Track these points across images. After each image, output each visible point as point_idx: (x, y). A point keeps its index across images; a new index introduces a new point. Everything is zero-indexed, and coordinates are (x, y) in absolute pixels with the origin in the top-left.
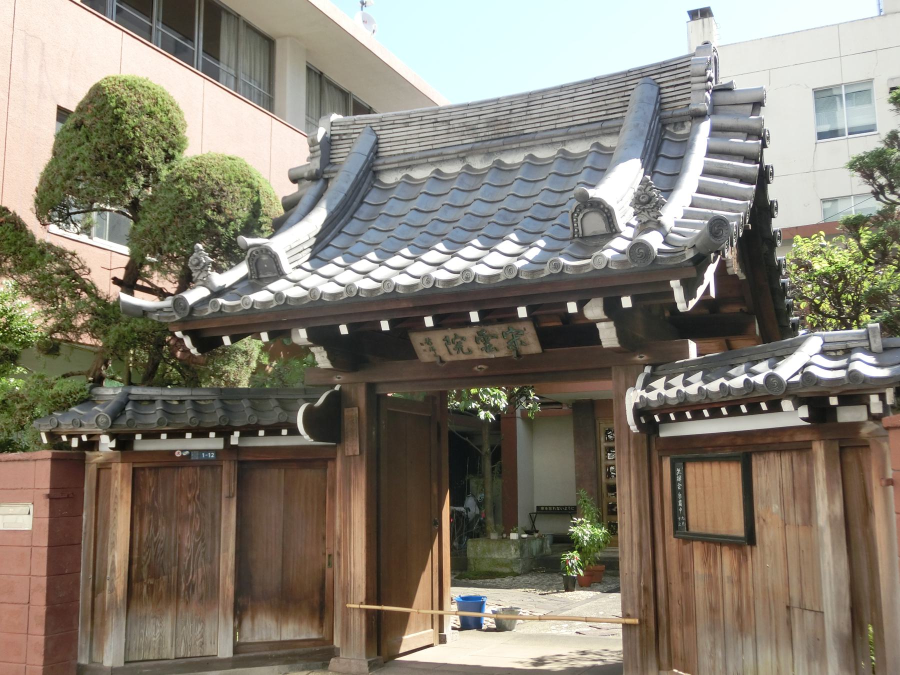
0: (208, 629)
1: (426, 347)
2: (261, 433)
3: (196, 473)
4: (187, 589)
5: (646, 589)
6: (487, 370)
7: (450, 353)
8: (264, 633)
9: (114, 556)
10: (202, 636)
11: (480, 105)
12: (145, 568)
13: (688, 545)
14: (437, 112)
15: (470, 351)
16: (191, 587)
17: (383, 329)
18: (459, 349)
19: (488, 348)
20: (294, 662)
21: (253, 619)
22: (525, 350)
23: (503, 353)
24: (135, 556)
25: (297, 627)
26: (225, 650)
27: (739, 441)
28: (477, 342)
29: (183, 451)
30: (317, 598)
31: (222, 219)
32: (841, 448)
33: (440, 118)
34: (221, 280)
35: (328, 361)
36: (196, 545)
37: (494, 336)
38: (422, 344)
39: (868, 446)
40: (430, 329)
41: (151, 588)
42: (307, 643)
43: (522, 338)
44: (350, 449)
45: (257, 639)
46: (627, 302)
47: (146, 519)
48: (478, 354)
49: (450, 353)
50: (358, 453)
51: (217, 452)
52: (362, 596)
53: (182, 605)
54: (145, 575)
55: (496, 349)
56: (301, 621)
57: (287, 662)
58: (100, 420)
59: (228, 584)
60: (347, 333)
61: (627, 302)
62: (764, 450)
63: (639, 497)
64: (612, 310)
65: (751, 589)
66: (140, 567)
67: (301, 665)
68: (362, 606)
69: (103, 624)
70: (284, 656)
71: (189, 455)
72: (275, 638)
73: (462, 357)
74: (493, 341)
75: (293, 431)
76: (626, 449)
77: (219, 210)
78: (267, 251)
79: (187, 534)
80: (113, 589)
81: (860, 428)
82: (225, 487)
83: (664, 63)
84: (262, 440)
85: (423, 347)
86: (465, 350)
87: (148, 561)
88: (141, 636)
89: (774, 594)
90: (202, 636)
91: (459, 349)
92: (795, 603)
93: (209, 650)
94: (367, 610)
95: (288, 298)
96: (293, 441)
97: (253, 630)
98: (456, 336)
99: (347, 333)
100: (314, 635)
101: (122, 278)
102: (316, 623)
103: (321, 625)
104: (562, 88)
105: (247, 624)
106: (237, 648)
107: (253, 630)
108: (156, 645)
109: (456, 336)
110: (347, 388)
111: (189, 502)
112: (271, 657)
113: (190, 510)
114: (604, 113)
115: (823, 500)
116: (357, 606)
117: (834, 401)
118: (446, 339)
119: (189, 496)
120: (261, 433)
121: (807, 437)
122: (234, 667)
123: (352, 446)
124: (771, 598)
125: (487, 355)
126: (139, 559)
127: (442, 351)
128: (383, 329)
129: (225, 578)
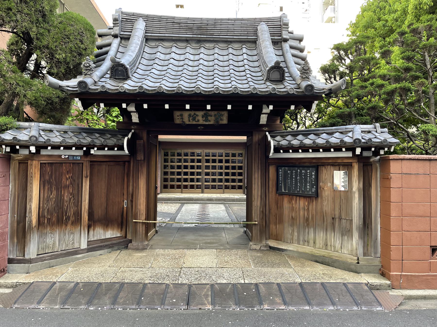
0: (76, 236)
1: (179, 117)
2: (49, 148)
3: (71, 166)
4: (66, 219)
6: (203, 129)
7: (189, 121)
8: (98, 236)
9: (31, 206)
10: (73, 240)
11: (194, 19)
12: (46, 210)
13: (281, 197)
15: (198, 121)
16: (68, 218)
17: (166, 108)
18: (194, 119)
20: (112, 247)
21: (94, 230)
23: (212, 123)
25: (112, 232)
26: (84, 246)
27: (314, 161)
28: (203, 118)
29: (65, 155)
32: (363, 165)
35: (138, 119)
36: (70, 199)
37: (211, 116)
38: (178, 116)
39: (372, 165)
40: (209, 110)
41: (49, 220)
42: (116, 238)
43: (222, 117)
44: (139, 157)
45: (95, 239)
46: (145, 106)
47: (46, 187)
48: (201, 122)
49: (189, 121)
50: (143, 159)
51: (81, 156)
52: (144, 217)
53: (64, 226)
54: (46, 214)
55: (210, 121)
56: (113, 230)
57: (110, 248)
58: (32, 138)
60: (168, 108)
61: (145, 106)
62: (324, 165)
63: (261, 179)
64: (139, 109)
65: (314, 212)
66: (44, 210)
68: (144, 221)
70: (109, 245)
71: (68, 158)
72: (103, 237)
73: (194, 123)
74: (209, 118)
75: (121, 148)
76: (257, 162)
77: (81, 41)
80: (31, 221)
81: (370, 159)
82: (84, 173)
83: (269, 18)
85: (178, 117)
86: (196, 120)
87: (48, 208)
88: (44, 242)
89: (326, 213)
90: (73, 240)
91: (194, 119)
92: (337, 216)
93: (76, 245)
94: (145, 223)
96: (120, 153)
97: (94, 235)
98: (195, 114)
99: (168, 108)
102: (120, 230)
103: (121, 230)
104: (229, 19)
105: (91, 232)
107: (94, 235)
108: (51, 246)
109: (195, 114)
110: (137, 131)
111: (67, 179)
112: (103, 246)
113: (68, 183)
114: (246, 33)
115: (356, 182)
116: (142, 221)
117: (18, 147)
119: (67, 176)
120: (106, 149)
121: (350, 161)
122: (87, 252)
124: (325, 215)
125: (205, 123)
126: (43, 206)
128: (166, 108)
129: (84, 213)
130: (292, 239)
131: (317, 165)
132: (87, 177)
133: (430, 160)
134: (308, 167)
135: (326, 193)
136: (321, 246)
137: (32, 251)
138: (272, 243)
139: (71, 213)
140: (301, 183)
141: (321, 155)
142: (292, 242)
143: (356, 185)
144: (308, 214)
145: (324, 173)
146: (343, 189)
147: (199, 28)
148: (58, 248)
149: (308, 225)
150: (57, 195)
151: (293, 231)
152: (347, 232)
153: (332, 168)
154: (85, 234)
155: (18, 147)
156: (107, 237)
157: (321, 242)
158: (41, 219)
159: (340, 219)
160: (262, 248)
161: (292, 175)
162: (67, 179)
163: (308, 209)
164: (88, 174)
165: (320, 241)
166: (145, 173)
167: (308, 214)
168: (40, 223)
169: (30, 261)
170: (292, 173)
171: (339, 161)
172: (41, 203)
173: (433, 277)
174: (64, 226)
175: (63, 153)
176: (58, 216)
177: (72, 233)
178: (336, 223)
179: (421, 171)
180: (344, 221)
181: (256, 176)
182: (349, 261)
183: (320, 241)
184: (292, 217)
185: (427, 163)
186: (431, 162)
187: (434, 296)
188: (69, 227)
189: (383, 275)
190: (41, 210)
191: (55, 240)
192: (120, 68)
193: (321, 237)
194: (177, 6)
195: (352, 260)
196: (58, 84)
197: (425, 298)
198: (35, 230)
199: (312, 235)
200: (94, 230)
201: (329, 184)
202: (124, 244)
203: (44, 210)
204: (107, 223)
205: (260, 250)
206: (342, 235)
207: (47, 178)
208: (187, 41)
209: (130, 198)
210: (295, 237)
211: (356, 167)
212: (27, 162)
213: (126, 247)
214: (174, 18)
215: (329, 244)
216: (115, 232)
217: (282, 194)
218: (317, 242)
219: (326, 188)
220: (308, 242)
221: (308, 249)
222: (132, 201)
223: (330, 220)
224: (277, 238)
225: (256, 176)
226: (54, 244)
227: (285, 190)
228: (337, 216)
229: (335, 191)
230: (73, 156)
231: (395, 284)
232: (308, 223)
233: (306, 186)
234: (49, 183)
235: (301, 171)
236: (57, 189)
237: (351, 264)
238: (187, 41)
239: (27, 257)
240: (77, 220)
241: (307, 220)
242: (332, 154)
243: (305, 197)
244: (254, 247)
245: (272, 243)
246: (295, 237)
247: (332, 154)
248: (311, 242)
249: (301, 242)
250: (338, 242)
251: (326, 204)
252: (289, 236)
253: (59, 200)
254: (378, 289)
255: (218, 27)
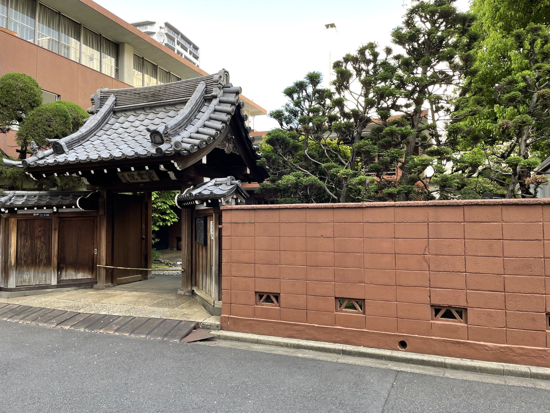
4: (39, 261)
5: (189, 260)
14: (136, 90)
15: (137, 179)
16: (41, 261)
19: (142, 178)
20: (80, 286)
21: (66, 271)
22: (154, 179)
23: (148, 180)
24: (19, 250)
26: (54, 282)
30: (91, 264)
31: (51, 129)
33: (137, 92)
34: (40, 154)
36: (42, 246)
41: (25, 261)
45: (67, 278)
47: (23, 238)
51: (50, 214)
52: (104, 263)
53: (37, 267)
56: (84, 273)
59: (55, 260)
67: (83, 287)
69: (8, 273)
72: (74, 278)
73: (135, 181)
75: (76, 207)
78: (58, 143)
79: (39, 243)
80: (11, 262)
82: (53, 226)
84: (64, 209)
91: (134, 178)
93: (48, 282)
95: (59, 162)
96: (76, 210)
97: (66, 275)
100: (90, 277)
101: (396, 104)
102: (91, 273)
103: (92, 273)
105: (64, 273)
106: (58, 282)
107: (66, 275)
111: (39, 231)
117: (16, 209)
118: (128, 175)
123: (101, 212)
126: (20, 251)
127: (128, 179)
132: (55, 230)
137: (12, 283)
139: (43, 256)
147: (153, 95)
148: (33, 283)
150: (32, 244)
154: (54, 274)
155: (16, 209)
156: (78, 278)
158: (19, 261)
160: (186, 294)
162: (39, 231)
164: (57, 227)
166: (105, 225)
169: (11, 290)
172: (19, 249)
173: (257, 323)
174: (37, 267)
175: (36, 212)
176: (32, 259)
177: (44, 272)
179: (247, 220)
181: (184, 227)
185: (252, 213)
186: (256, 211)
187: (246, 339)
188: (41, 268)
190: (19, 254)
191: (31, 277)
192: (58, 145)
194: (327, 26)
196: (11, 164)
197: (238, 340)
198: (14, 268)
200: (66, 271)
202: (89, 285)
203: (21, 254)
204: (77, 266)
207: (23, 230)
213: (92, 287)
216: (86, 274)
226: (30, 279)
230: (43, 214)
231: (224, 325)
234: (25, 234)
236: (32, 239)
239: (9, 287)
240: (48, 263)
253: (33, 247)
254: (208, 329)
255: (168, 91)
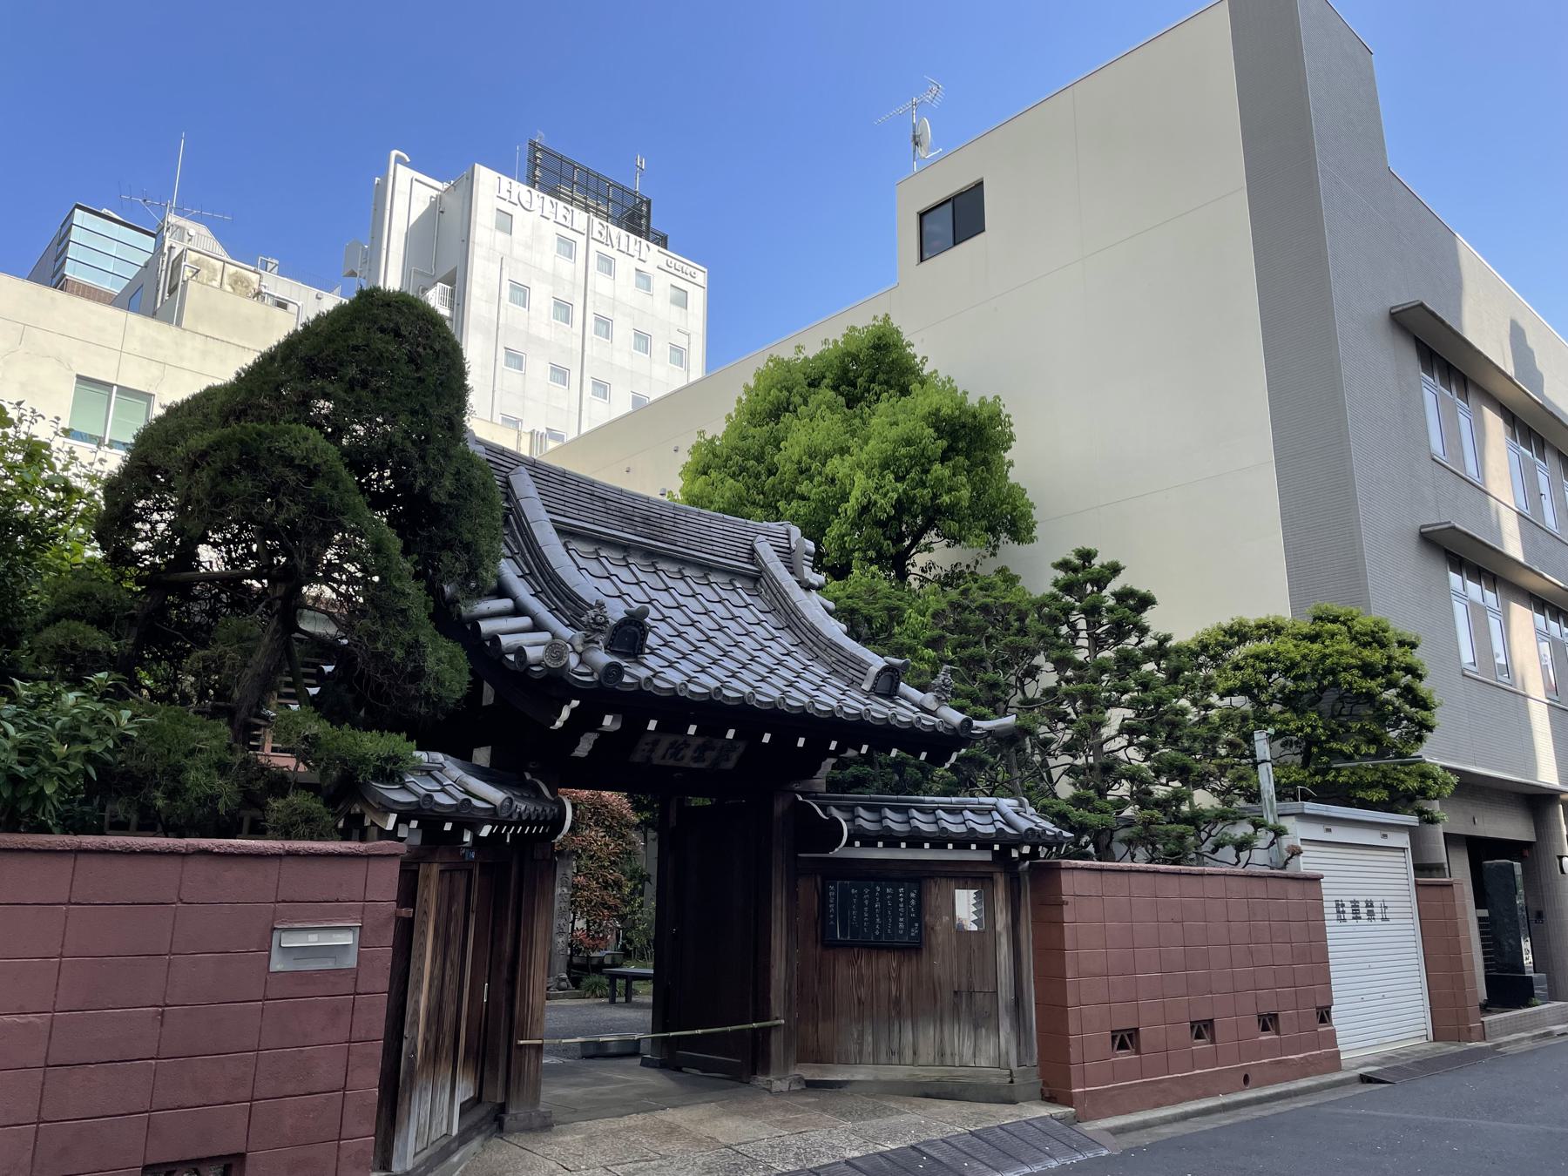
92: (964, 988)
130: (861, 1052)
131: (921, 875)
133: (1179, 874)
134: (900, 881)
135: (940, 937)
136: (931, 1059)
138: (811, 1073)
140: (883, 915)
141: (927, 854)
142: (860, 1062)
143: (1002, 920)
144: (899, 989)
145: (935, 893)
146: (974, 928)
149: (899, 1013)
151: (861, 1035)
152: (982, 1021)
153: (953, 884)
157: (931, 1050)
159: (971, 993)
161: (861, 899)
163: (899, 976)
165: (927, 1051)
167: (899, 989)
168: (433, 1055)
170: (861, 894)
171: (968, 869)
178: (967, 1004)
180: (979, 997)
181: (779, 901)
182: (994, 1080)
183: (927, 1051)
184: (859, 999)
189: (1050, 1098)
193: (928, 1039)
195: (998, 1078)
199: (908, 1036)
201: (946, 919)
205: (790, 1092)
206: (976, 1027)
208: (625, 548)
209: (505, 974)
210: (868, 1048)
211: (1001, 881)
212: (414, 867)
214: (592, 483)
215: (948, 1052)
217: (829, 944)
218: (922, 1049)
219: (938, 928)
220: (900, 1054)
221: (899, 1072)
222: (512, 983)
223: (947, 996)
224: (818, 1056)
225: (779, 901)
227: (843, 933)
228: (964, 988)
229: (961, 932)
232: (898, 1011)
233: (895, 923)
235: (907, 894)
237: (999, 1087)
238: (625, 548)
241: (898, 1001)
242: (950, 854)
243: (890, 948)
244: (778, 1085)
245: (811, 1073)
246: (868, 1048)
247: (950, 854)
248: (908, 1053)
249: (883, 1057)
250: (967, 1043)
251: (942, 963)
252: (853, 1048)
